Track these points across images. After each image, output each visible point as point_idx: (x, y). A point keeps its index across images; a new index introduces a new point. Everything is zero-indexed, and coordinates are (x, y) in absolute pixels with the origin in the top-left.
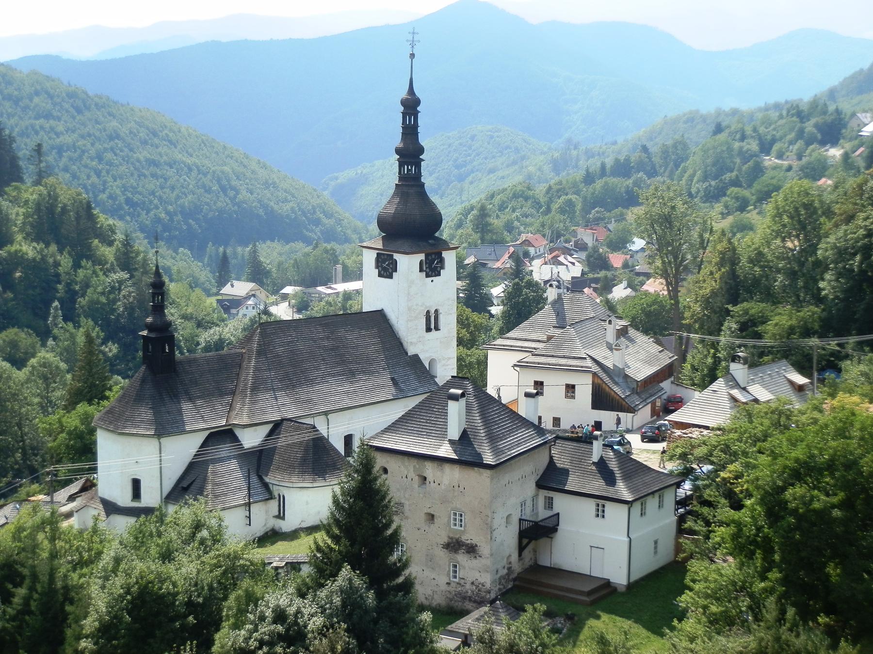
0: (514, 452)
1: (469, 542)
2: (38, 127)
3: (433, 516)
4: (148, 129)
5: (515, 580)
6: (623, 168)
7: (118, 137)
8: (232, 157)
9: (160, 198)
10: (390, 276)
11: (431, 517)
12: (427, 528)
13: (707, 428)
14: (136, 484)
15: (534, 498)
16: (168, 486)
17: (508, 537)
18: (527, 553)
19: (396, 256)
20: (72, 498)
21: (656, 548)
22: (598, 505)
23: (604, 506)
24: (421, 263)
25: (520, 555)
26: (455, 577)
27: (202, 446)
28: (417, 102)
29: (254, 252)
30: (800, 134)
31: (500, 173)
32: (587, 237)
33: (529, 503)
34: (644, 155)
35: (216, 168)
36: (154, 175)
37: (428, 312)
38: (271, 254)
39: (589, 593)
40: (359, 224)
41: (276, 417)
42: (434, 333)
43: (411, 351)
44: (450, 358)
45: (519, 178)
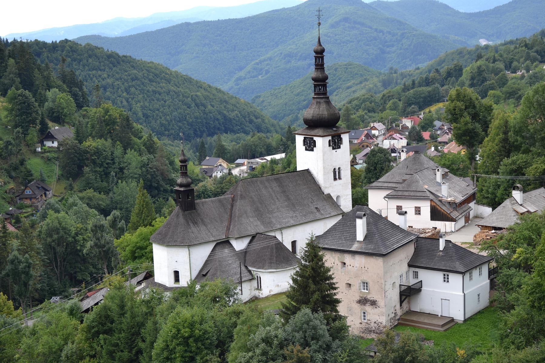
0: (395, 246)
1: (372, 299)
2: (91, 76)
3: (350, 285)
4: (153, 73)
5: (399, 320)
6: (427, 82)
7: (137, 79)
8: (201, 88)
9: (162, 112)
10: (312, 150)
11: (349, 285)
12: (347, 292)
13: (500, 229)
14: (176, 273)
15: (407, 273)
16: (195, 273)
17: (394, 295)
18: (405, 304)
20: (139, 283)
21: (479, 298)
22: (445, 275)
23: (448, 275)
24: (330, 141)
25: (401, 305)
26: (365, 319)
27: (212, 251)
28: (323, 51)
29: (219, 140)
30: (528, 57)
31: (353, 89)
32: (408, 123)
33: (404, 276)
34: (436, 74)
35: (193, 93)
36: (158, 100)
37: (335, 169)
38: (227, 141)
39: (443, 326)
40: (275, 122)
41: (253, 232)
42: (338, 181)
43: (326, 192)
45: (363, 92)
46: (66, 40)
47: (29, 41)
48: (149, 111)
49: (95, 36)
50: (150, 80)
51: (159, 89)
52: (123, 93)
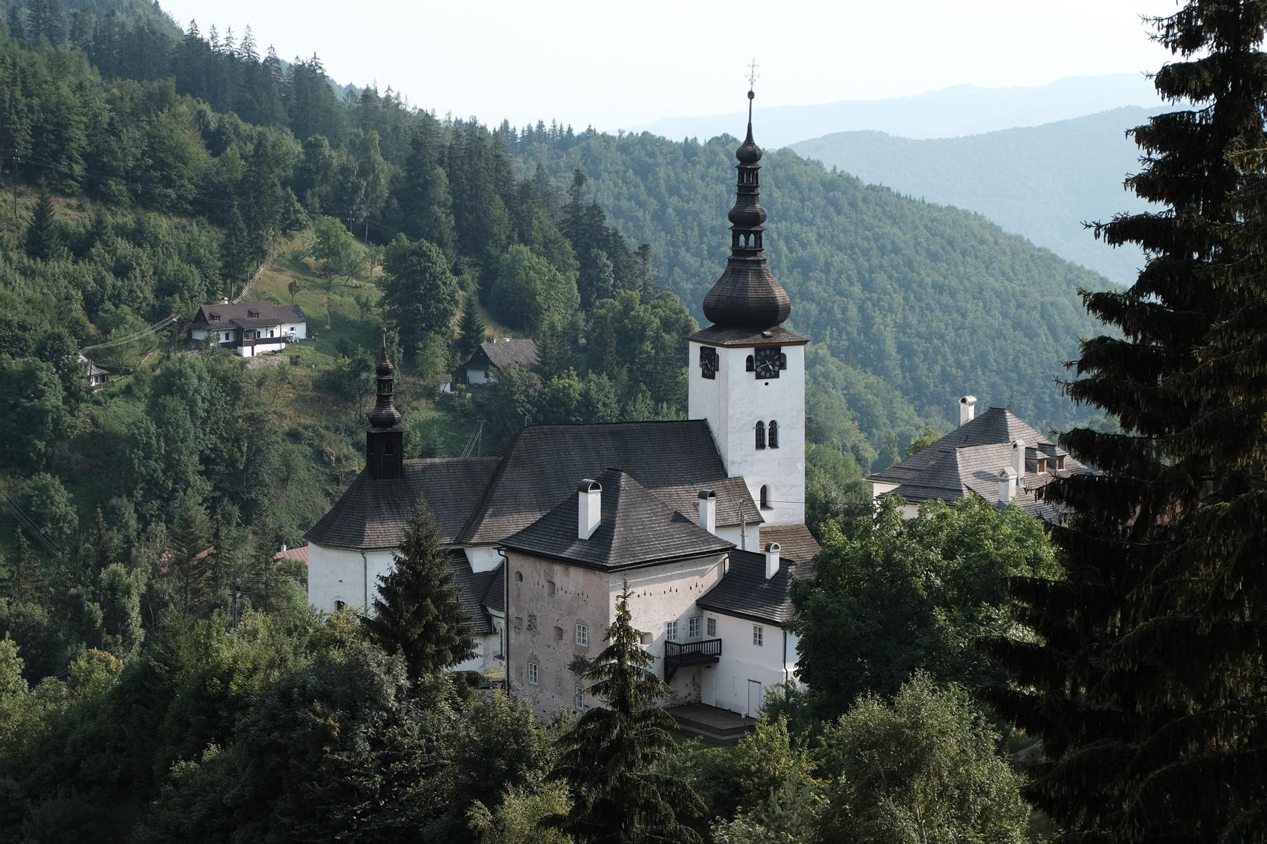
7: (896, 250)
19: (719, 350)
24: (749, 359)
37: (760, 424)
44: (793, 486)
46: (726, 136)
47: (625, 135)
48: (916, 340)
49: (871, 133)
50: (934, 257)
51: (953, 282)
52: (852, 284)
